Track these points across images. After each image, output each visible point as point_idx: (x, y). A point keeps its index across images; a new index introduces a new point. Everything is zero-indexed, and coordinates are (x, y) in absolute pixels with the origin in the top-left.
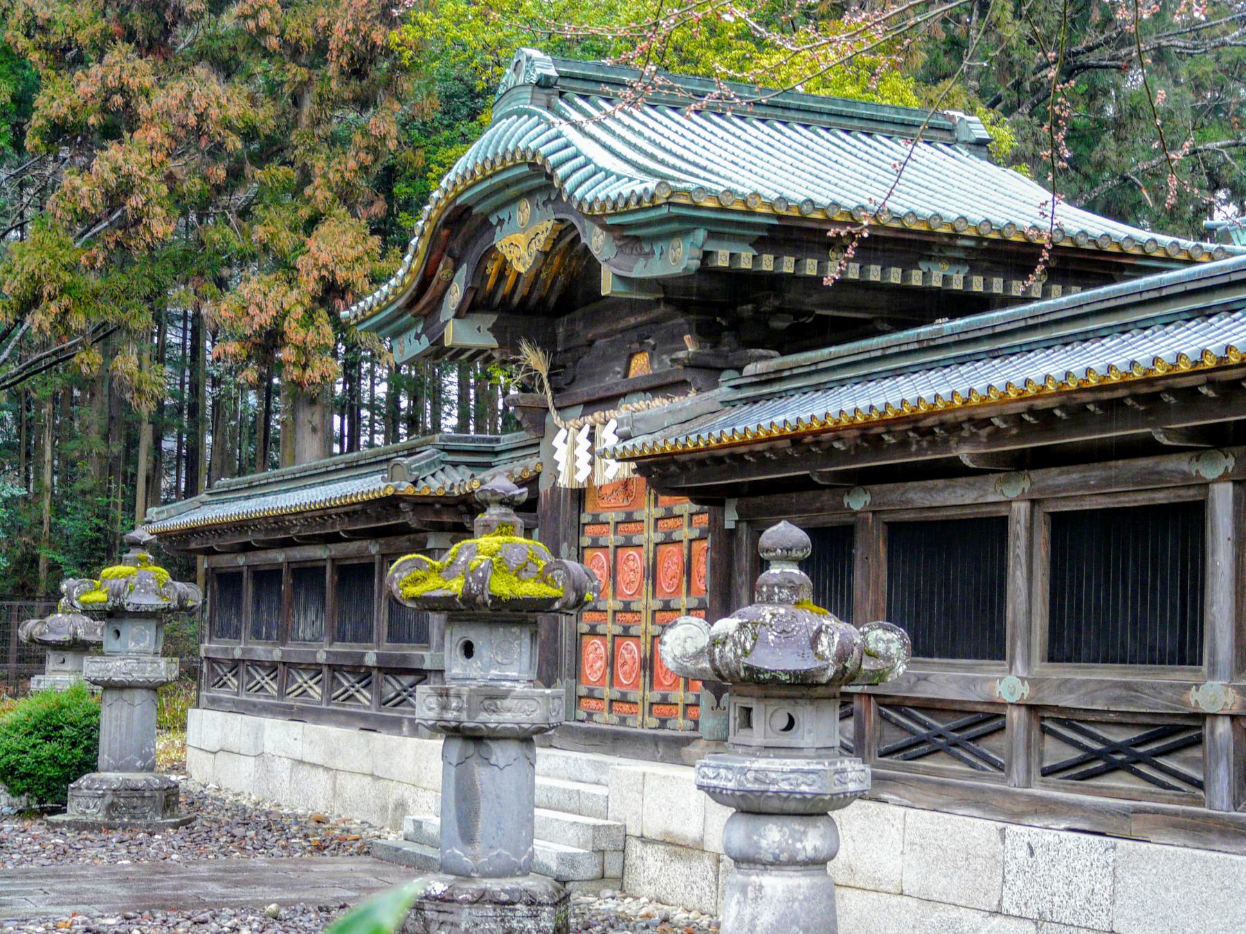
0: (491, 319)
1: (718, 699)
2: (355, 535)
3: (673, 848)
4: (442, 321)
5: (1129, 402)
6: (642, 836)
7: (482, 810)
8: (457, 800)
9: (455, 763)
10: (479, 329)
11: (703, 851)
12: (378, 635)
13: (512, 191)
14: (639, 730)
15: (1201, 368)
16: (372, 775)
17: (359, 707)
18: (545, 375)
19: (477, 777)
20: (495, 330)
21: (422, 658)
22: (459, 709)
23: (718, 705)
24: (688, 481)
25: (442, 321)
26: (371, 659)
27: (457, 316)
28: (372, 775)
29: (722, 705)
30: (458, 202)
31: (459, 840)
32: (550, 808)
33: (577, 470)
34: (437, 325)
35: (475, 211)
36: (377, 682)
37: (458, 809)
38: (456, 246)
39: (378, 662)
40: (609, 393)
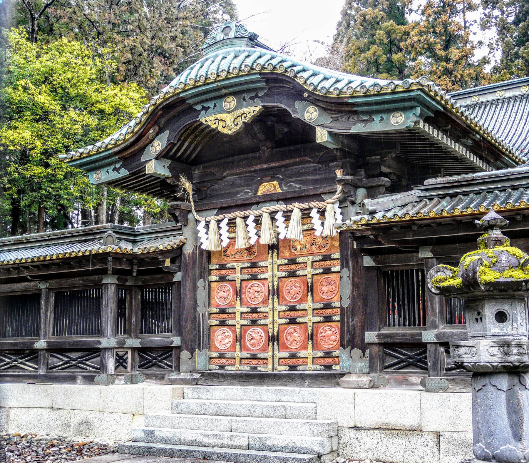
0: (169, 162)
1: (364, 353)
2: (36, 278)
3: (390, 432)
4: (143, 160)
5: (31, 267)
6: (356, 427)
7: (525, 419)
8: (509, 413)
9: (505, 389)
10: (164, 166)
11: (421, 431)
12: (45, 331)
13: (224, 91)
14: (271, 372)
15: (427, 217)
16: (52, 408)
17: (24, 372)
18: (191, 193)
19: (521, 398)
20: (170, 168)
21: (100, 343)
22: (519, 354)
23: (364, 355)
24: (413, 236)
25: (143, 160)
26: (41, 344)
27: (157, 158)
28: (52, 408)
29: (366, 355)
30: (181, 95)
31: (512, 439)
32: (213, 415)
33: (250, 238)
34: (138, 162)
35: (187, 102)
36: (44, 357)
37: (510, 419)
38: (163, 120)
39: (48, 346)
40: (247, 202)
